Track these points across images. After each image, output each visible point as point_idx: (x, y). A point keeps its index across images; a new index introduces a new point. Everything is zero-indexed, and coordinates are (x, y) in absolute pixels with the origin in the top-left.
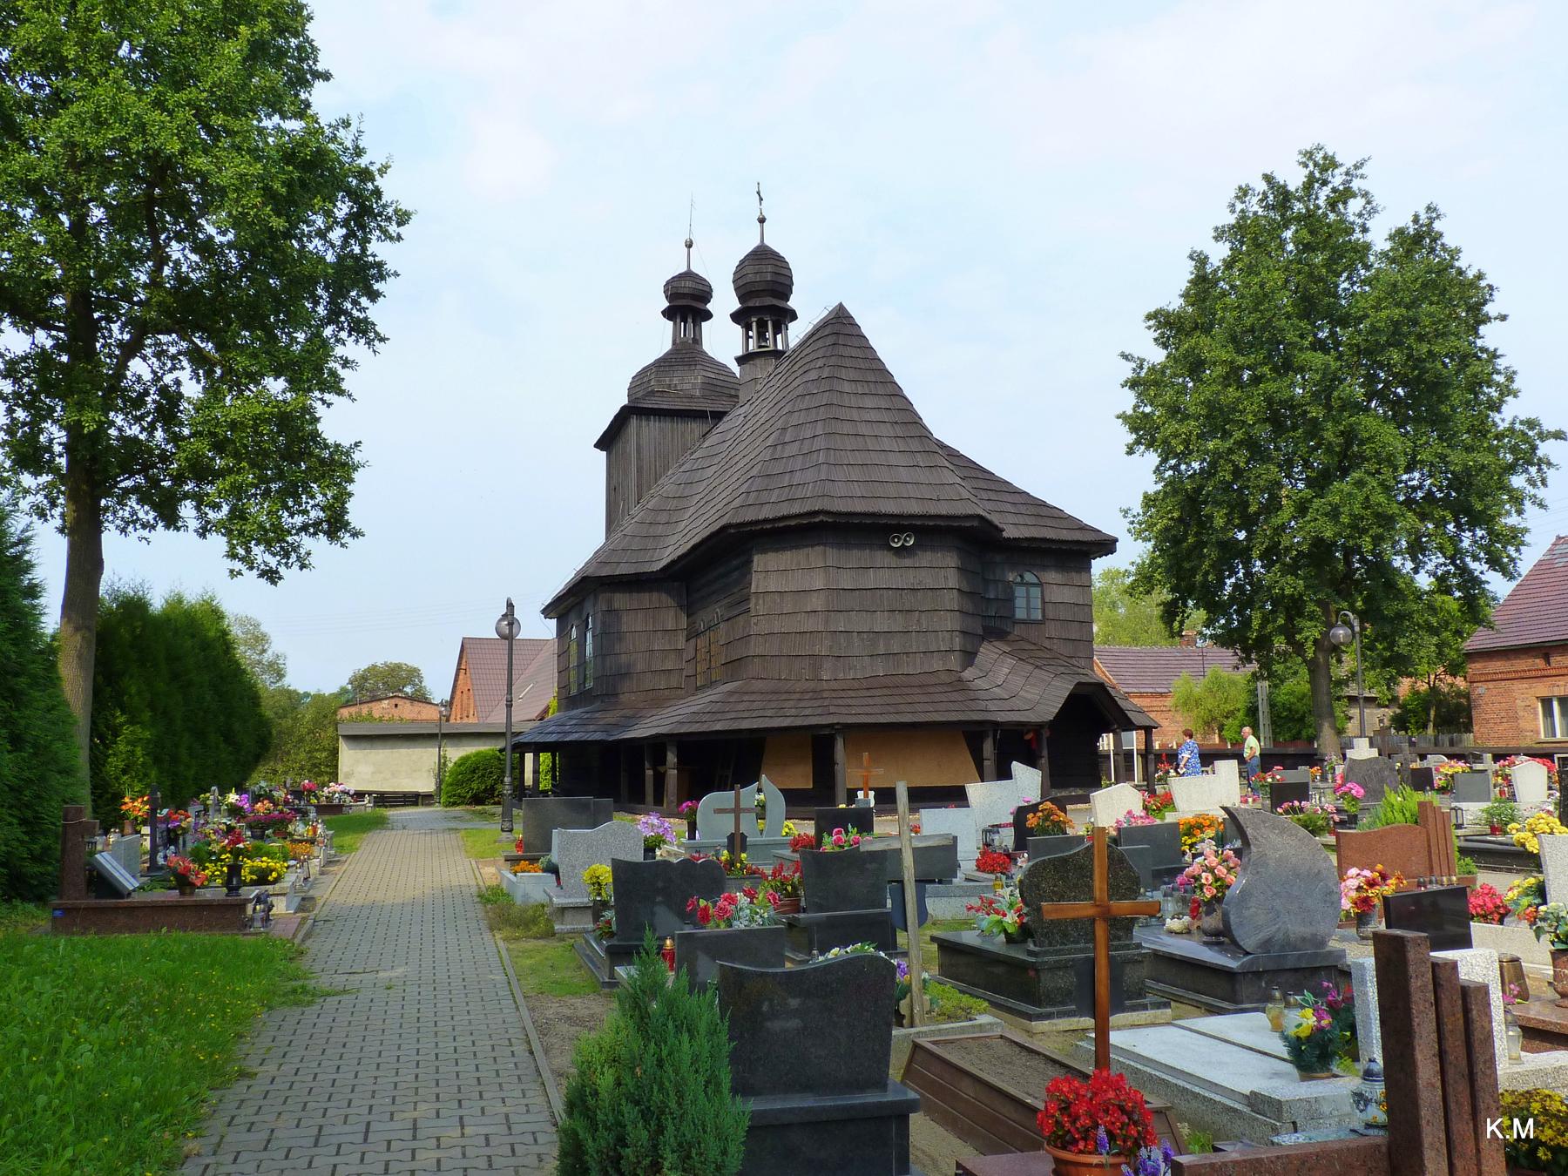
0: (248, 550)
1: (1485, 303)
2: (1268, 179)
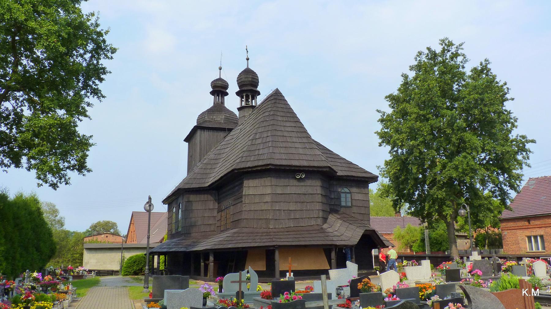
0: (45, 176)
1: (506, 94)
2: (429, 49)
